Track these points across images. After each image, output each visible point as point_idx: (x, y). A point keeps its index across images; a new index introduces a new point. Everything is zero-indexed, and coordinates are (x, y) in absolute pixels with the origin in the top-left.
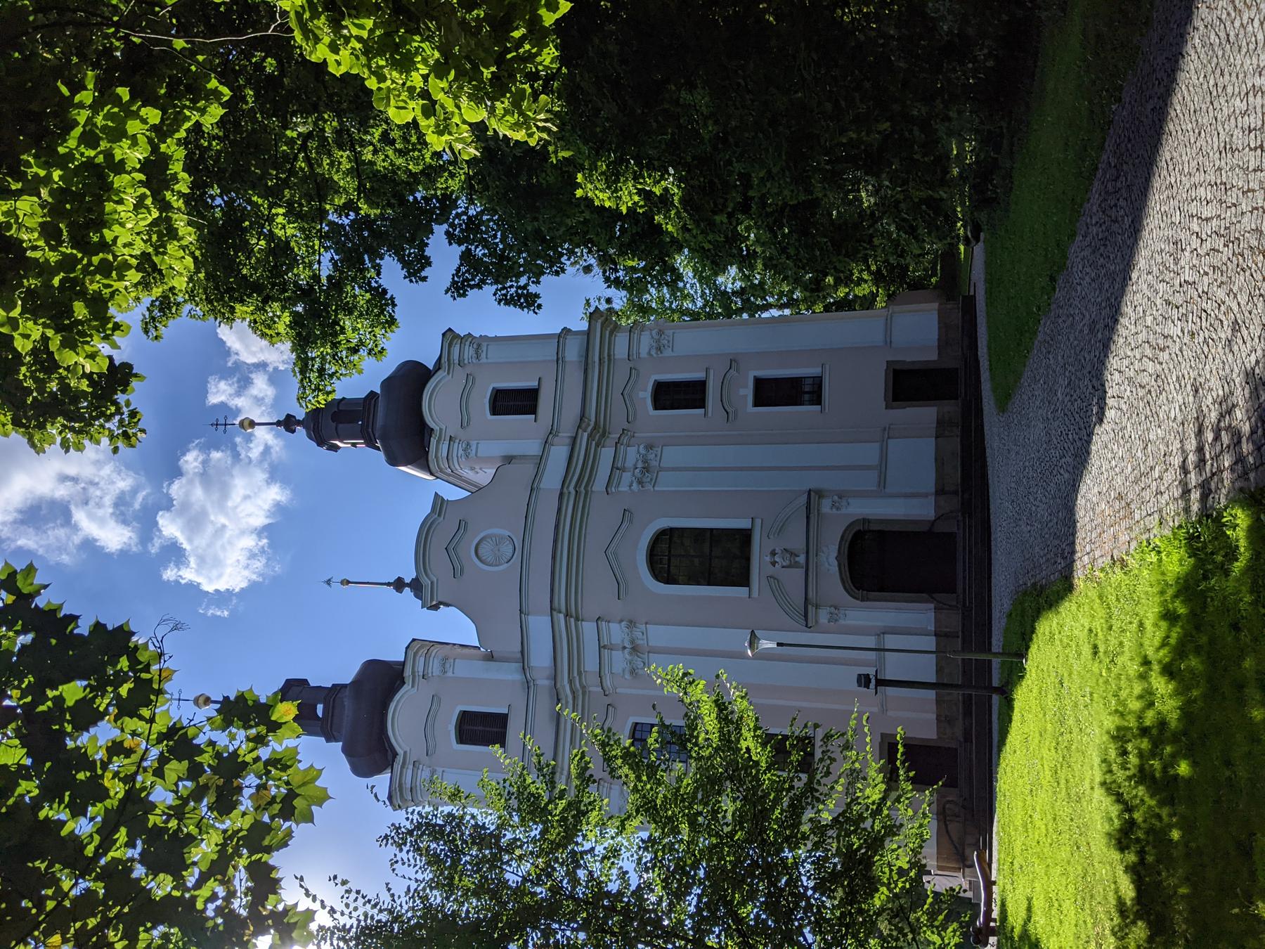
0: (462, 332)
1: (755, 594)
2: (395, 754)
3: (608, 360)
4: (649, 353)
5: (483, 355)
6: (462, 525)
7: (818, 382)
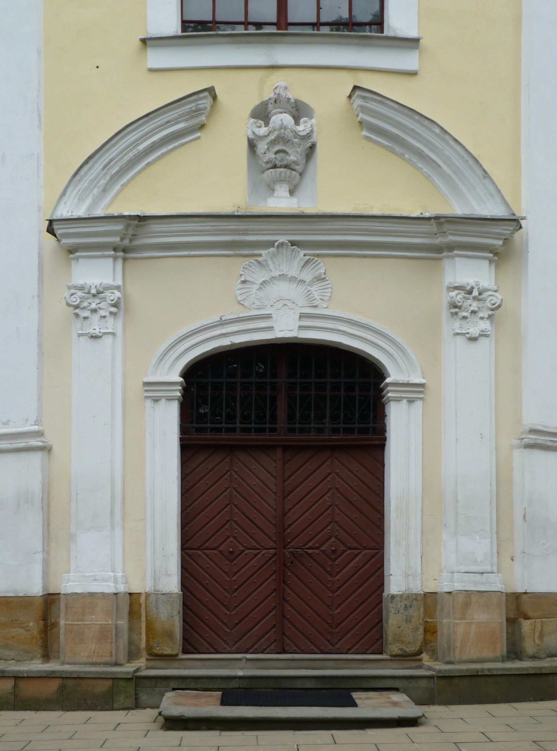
1: (158, 58)
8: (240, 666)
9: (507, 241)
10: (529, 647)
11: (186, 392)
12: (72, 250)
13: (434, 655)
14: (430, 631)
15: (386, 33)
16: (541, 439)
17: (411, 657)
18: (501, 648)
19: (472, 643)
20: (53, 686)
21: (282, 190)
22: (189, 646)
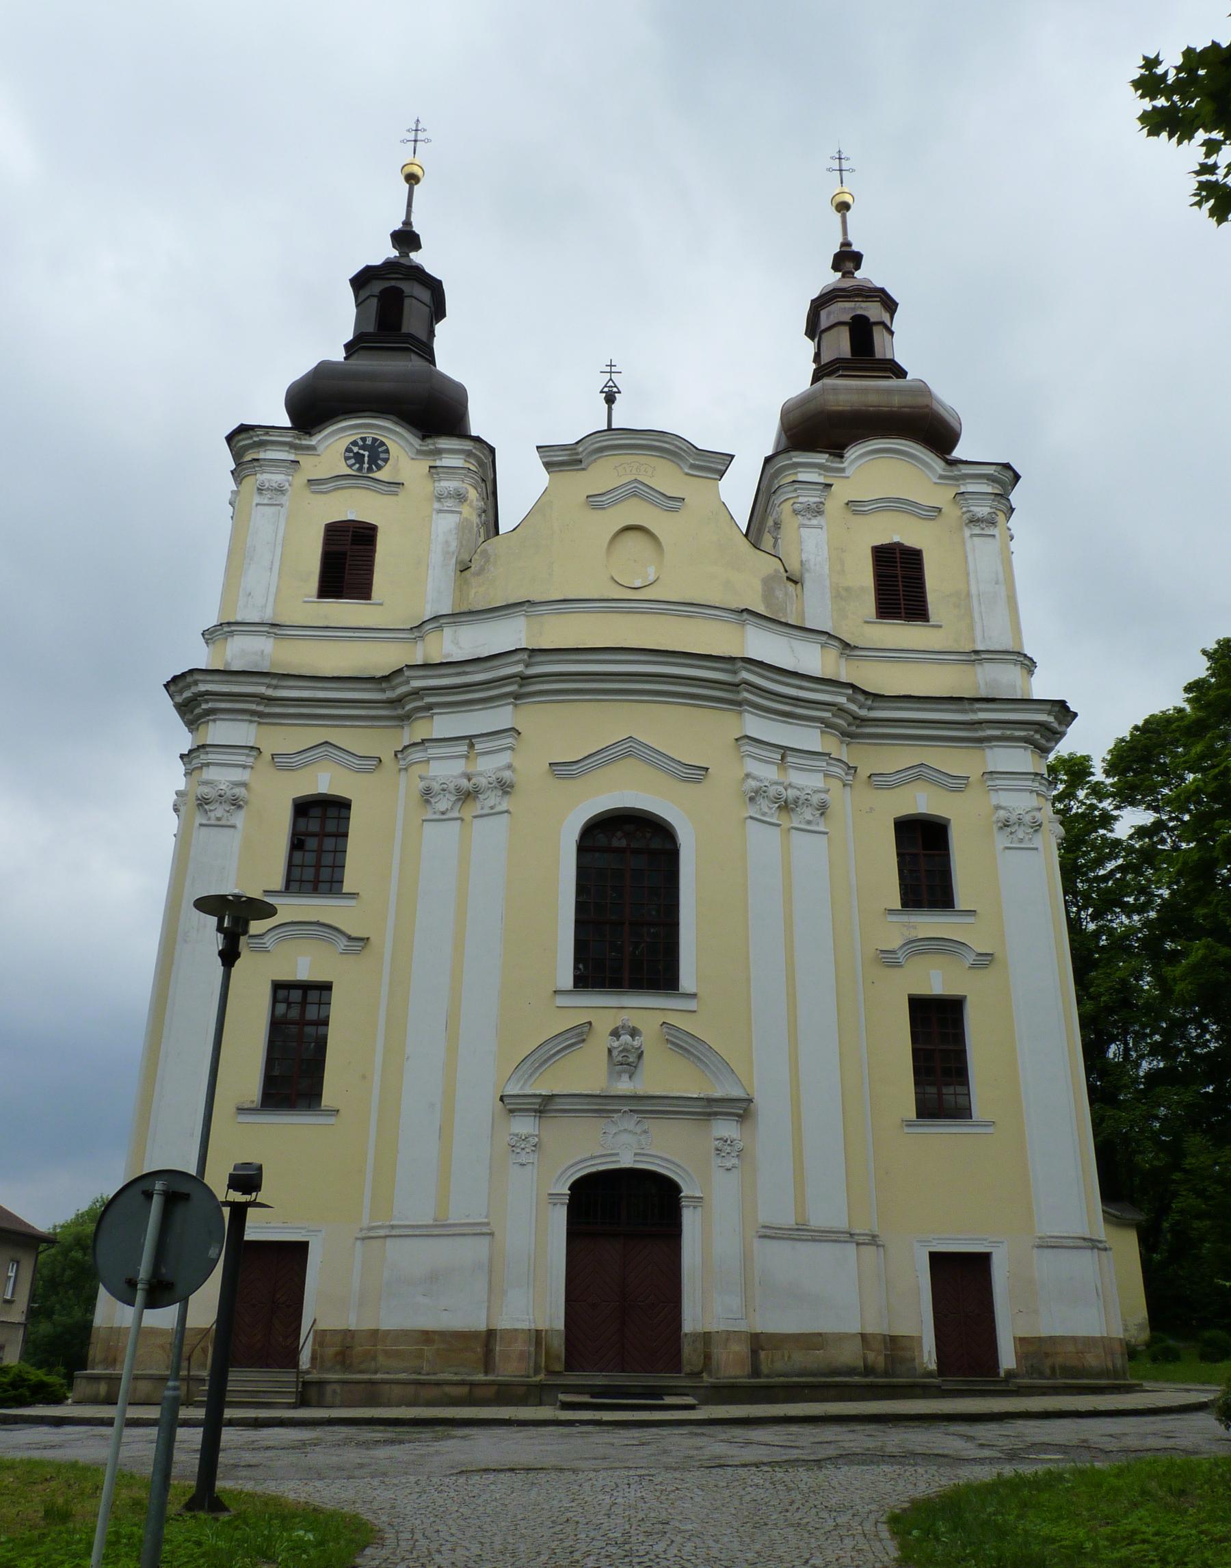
0: (1015, 497)
1: (561, 1001)
2: (310, 434)
3: (976, 735)
4: (998, 808)
5: (977, 531)
6: (673, 503)
7: (960, 1112)
8: (600, 1380)
9: (745, 1110)
10: (765, 1369)
11: (571, 1197)
12: (511, 1111)
13: (710, 1375)
14: (708, 1357)
15: (681, 990)
16: (769, 1232)
17: (697, 1375)
18: (748, 1369)
19: (731, 1364)
20: (493, 1389)
21: (625, 1077)
22: (569, 1367)
